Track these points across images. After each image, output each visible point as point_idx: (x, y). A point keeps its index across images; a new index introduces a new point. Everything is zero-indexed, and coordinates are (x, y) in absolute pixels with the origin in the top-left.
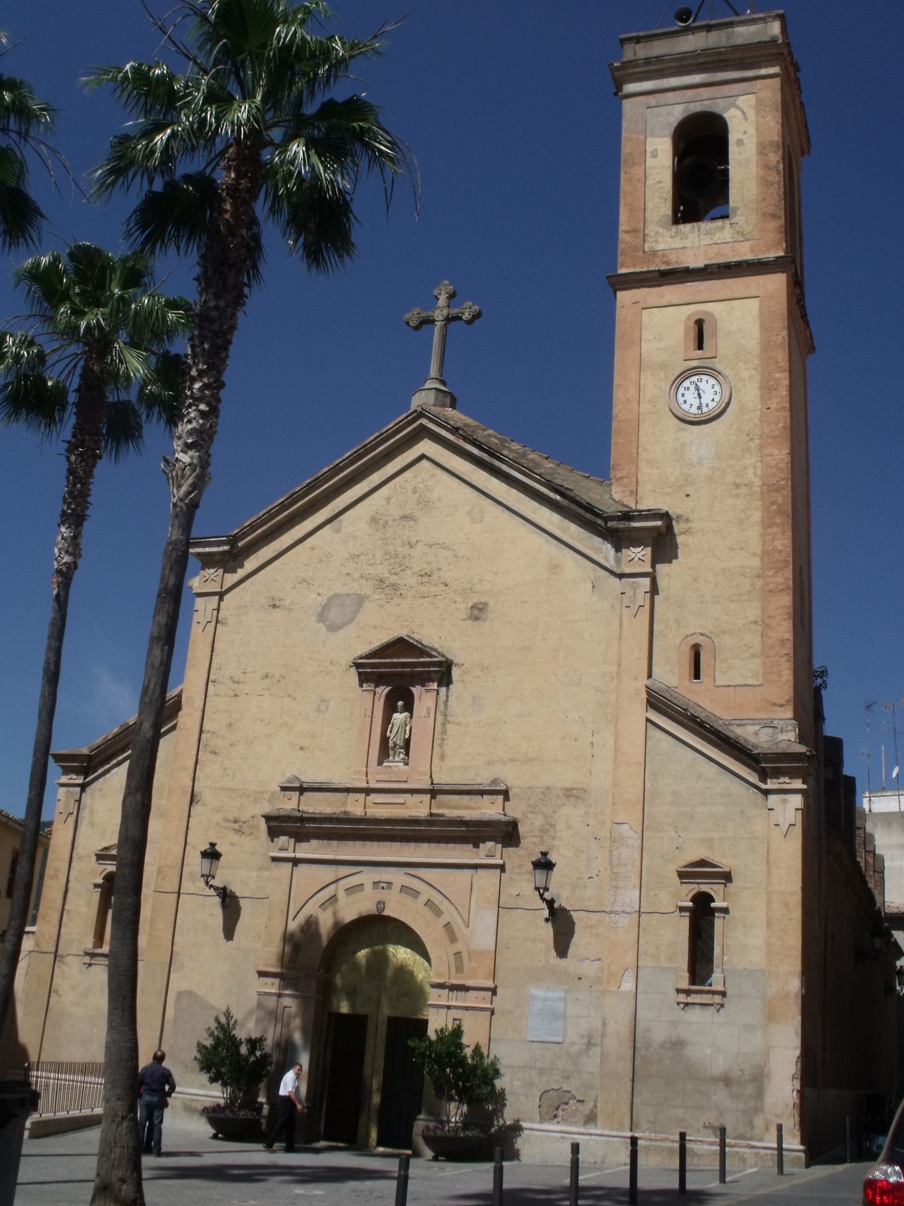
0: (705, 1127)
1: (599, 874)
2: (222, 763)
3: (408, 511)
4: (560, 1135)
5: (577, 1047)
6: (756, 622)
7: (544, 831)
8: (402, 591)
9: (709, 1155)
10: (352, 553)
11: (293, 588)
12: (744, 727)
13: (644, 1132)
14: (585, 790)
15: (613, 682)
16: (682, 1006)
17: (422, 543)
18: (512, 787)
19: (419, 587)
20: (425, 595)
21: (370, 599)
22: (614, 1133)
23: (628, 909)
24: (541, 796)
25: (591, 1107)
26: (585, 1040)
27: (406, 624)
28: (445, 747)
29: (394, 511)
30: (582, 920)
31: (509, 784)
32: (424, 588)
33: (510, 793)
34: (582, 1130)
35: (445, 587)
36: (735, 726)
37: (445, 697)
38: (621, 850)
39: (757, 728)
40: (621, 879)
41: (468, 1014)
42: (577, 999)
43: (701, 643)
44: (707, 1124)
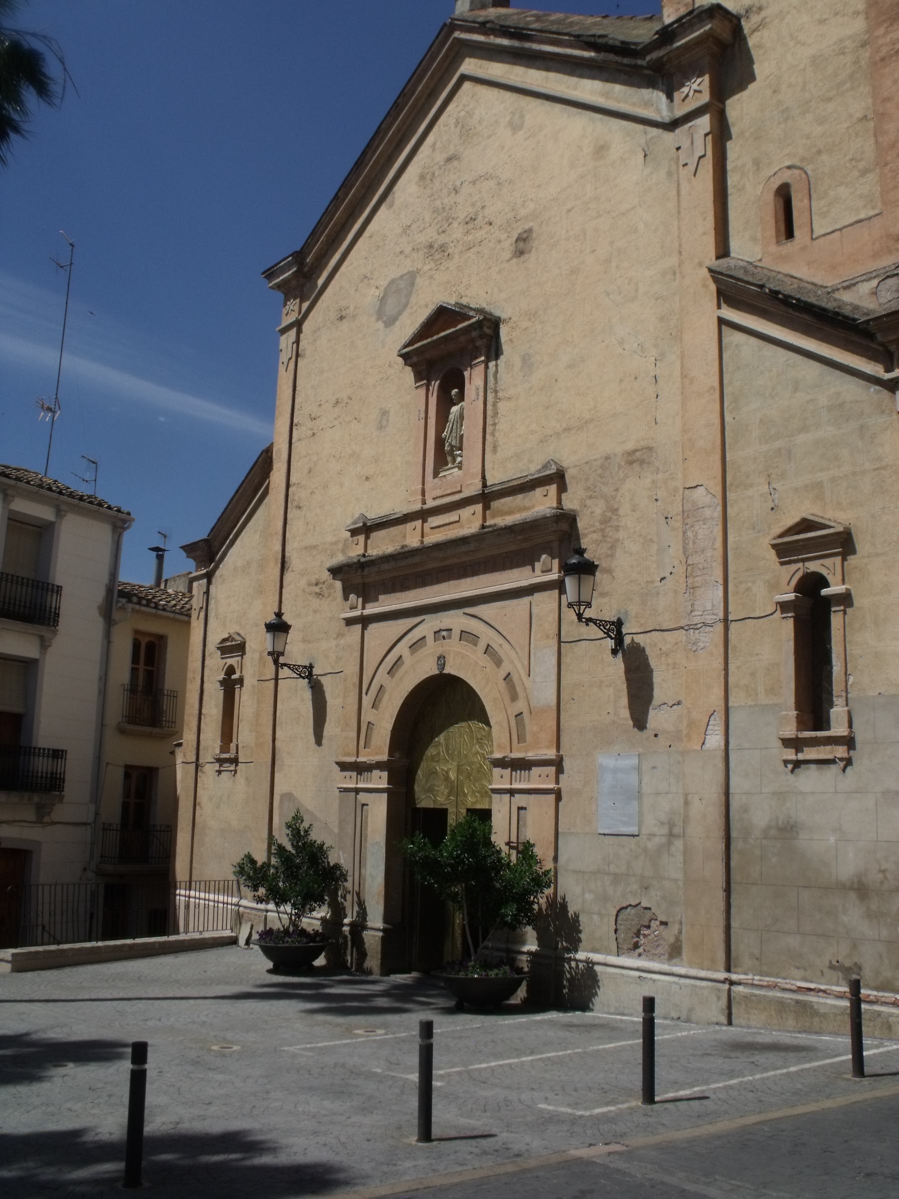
0: (832, 967)
1: (674, 571)
2: (305, 516)
3: (451, 151)
4: (637, 974)
5: (657, 840)
6: (866, 116)
7: (605, 521)
8: (450, 251)
9: (835, 1015)
10: (404, 225)
11: (356, 290)
12: (854, 288)
13: (746, 974)
14: (650, 449)
15: (675, 280)
16: (790, 766)
17: (466, 183)
18: (568, 468)
19: (465, 238)
20: (471, 246)
21: (421, 272)
22: (703, 974)
23: (709, 619)
24: (600, 471)
25: (676, 932)
26: (665, 830)
27: (454, 289)
28: (497, 434)
29: (440, 158)
30: (655, 645)
31: (565, 464)
32: (470, 237)
33: (567, 476)
34: (665, 967)
35: (490, 227)
36: (841, 291)
37: (494, 368)
38: (696, 528)
39: (874, 283)
40: (699, 573)
41: (532, 798)
42: (654, 768)
43: (789, 181)
44: (834, 963)
